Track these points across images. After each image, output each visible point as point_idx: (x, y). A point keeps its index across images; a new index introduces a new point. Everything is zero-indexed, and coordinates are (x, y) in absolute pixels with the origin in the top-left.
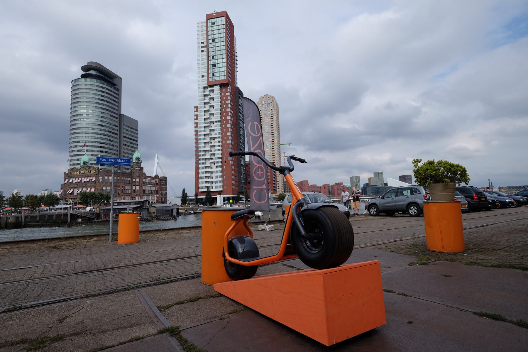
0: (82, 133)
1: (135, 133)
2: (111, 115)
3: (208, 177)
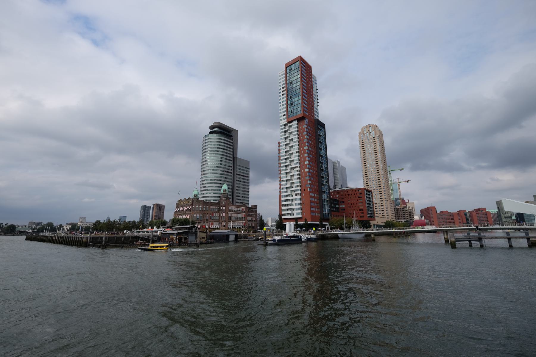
0: (208, 173)
1: (246, 171)
2: (226, 159)
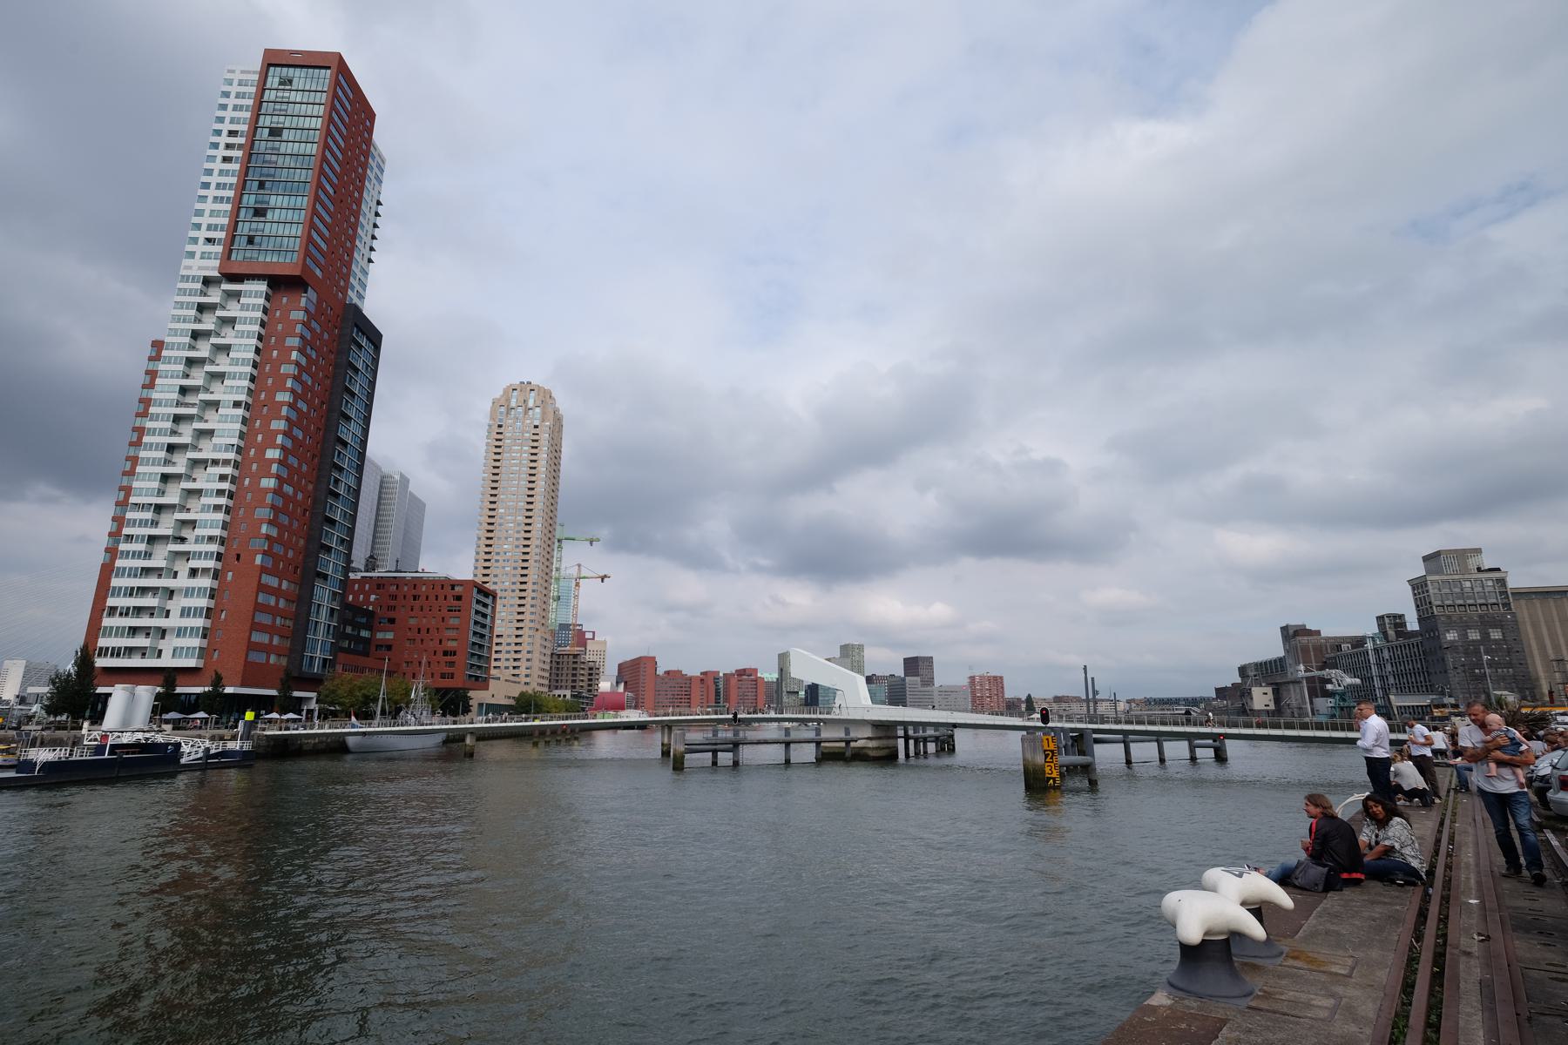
3: (150, 611)
